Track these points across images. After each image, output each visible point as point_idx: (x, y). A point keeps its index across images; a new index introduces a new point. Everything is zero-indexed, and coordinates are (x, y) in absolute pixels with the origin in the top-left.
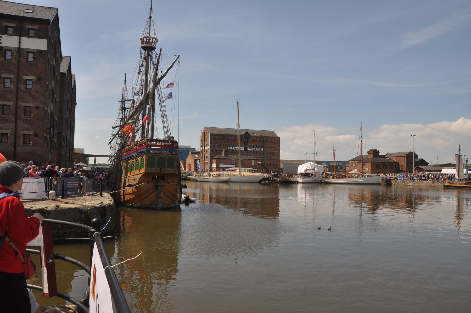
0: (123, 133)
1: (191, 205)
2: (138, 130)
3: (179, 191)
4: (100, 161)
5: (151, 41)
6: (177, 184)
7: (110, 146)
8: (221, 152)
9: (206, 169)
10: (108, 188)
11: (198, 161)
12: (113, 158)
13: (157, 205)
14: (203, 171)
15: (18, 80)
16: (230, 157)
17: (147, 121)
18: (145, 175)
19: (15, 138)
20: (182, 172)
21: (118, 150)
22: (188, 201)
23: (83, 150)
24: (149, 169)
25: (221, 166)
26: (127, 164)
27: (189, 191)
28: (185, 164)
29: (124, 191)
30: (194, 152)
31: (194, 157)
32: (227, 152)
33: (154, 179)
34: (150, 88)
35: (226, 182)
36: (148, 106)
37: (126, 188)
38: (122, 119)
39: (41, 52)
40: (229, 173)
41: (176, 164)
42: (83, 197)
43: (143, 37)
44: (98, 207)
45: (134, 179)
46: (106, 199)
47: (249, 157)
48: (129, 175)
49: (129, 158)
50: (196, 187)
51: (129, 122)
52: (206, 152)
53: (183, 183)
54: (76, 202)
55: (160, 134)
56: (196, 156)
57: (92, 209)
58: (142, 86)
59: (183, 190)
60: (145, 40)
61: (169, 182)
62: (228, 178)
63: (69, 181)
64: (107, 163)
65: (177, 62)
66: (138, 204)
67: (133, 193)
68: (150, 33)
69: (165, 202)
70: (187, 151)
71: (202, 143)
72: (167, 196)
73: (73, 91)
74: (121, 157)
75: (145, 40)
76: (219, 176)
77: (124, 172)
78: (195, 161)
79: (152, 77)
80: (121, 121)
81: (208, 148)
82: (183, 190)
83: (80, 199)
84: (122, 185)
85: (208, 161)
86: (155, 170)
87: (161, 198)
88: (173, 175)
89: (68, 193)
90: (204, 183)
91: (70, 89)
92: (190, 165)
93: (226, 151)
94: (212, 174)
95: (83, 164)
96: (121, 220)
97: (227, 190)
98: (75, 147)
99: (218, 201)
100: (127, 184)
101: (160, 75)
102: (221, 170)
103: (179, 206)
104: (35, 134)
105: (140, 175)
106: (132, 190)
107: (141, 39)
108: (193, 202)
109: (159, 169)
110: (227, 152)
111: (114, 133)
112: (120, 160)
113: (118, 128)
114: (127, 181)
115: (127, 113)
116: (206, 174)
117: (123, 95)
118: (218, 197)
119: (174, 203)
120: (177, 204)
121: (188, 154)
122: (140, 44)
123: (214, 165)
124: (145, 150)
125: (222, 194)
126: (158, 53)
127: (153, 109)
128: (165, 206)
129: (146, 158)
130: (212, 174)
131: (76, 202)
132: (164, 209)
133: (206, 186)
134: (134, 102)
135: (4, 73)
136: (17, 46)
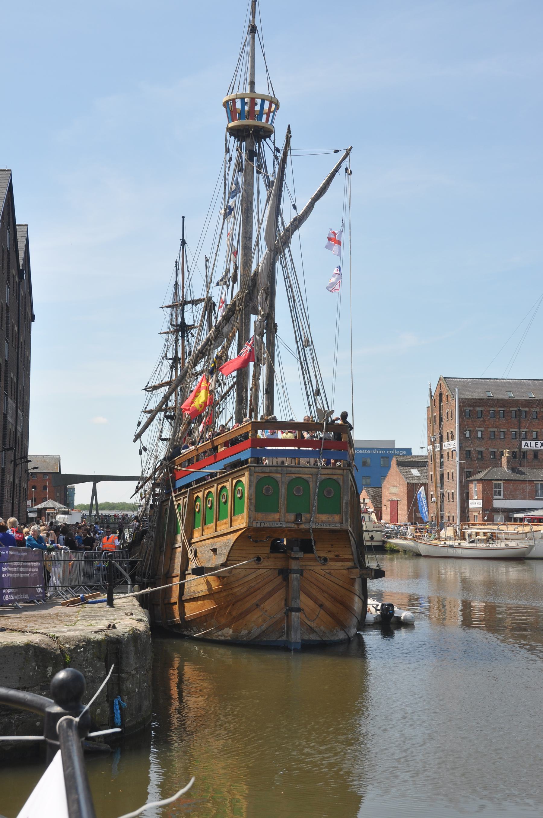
0: (175, 406)
1: (401, 635)
2: (228, 392)
3: (357, 587)
4: (108, 493)
5: (257, 108)
6: (350, 564)
7: (138, 445)
8: (496, 458)
9: (446, 515)
10: (132, 577)
11: (422, 489)
12: (148, 486)
13: (288, 633)
14: (440, 523)
16: (530, 473)
17: (252, 364)
18: (249, 537)
20: (366, 525)
21: (165, 459)
22: (388, 623)
23: (57, 460)
24: (260, 516)
25: (498, 503)
26: (193, 502)
27: (393, 586)
28: (377, 499)
29: (182, 587)
30: (407, 460)
31: (407, 476)
32: (519, 459)
33: (275, 548)
34: (257, 263)
35: (519, 558)
36: (253, 318)
37: (189, 578)
38: (175, 360)
40: (527, 529)
41: (346, 498)
42: (52, 611)
43: (232, 97)
44: (98, 643)
45: (214, 550)
46: (126, 616)
48: (197, 536)
49: (197, 481)
50: (417, 575)
51: (199, 368)
52: (445, 459)
53: (372, 563)
54: (31, 626)
55: (292, 405)
56: (415, 472)
57: (78, 646)
58: (236, 253)
59: (373, 585)
60: (238, 105)
61: (325, 559)
62: (524, 544)
63: (10, 559)
64: (132, 501)
65: (342, 170)
66: (229, 632)
67: (210, 595)
68: (252, 84)
69: (313, 625)
70: (384, 457)
71: (431, 430)
72: (321, 606)
73: (21, 277)
74: (174, 480)
75: (238, 105)
76: (493, 537)
77: (181, 527)
78: (412, 489)
79: (265, 223)
80: (173, 367)
81: (452, 445)
82: (373, 585)
83: (41, 616)
84: (177, 569)
85: (453, 487)
86: (280, 519)
87: (299, 610)
88: (338, 536)
89: (6, 598)
90: (441, 561)
91: (13, 271)
92: (394, 504)
93: (514, 455)
94: (468, 531)
95: (58, 505)
96: (174, 692)
97: (520, 587)
98: (30, 453)
99: (492, 622)
100: (192, 565)
101: (288, 216)
102: (499, 518)
103: (360, 638)
105: (233, 538)
106: (208, 583)
107: (226, 104)
108: (407, 625)
109: (291, 517)
110: (519, 459)
111: (152, 406)
112: (168, 489)
113: (165, 390)
114: (191, 556)
115: (193, 343)
116: (449, 531)
117: (176, 285)
118: (490, 609)
119: (343, 627)
120: (353, 631)
121: (389, 467)
122: (222, 121)
123: (476, 503)
124: (246, 455)
125: (505, 601)
126: (281, 145)
127: (270, 326)
128: (313, 637)
129: (250, 480)
130: (468, 531)
131: (31, 626)
132: (309, 647)
133: (450, 571)
134: (210, 306)
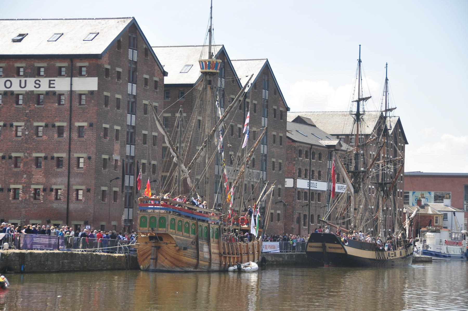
15: (70, 128)
19: (68, 194)
39: (92, 92)
47: (397, 212)
104: (87, 189)
135: (57, 121)
136: (69, 89)
